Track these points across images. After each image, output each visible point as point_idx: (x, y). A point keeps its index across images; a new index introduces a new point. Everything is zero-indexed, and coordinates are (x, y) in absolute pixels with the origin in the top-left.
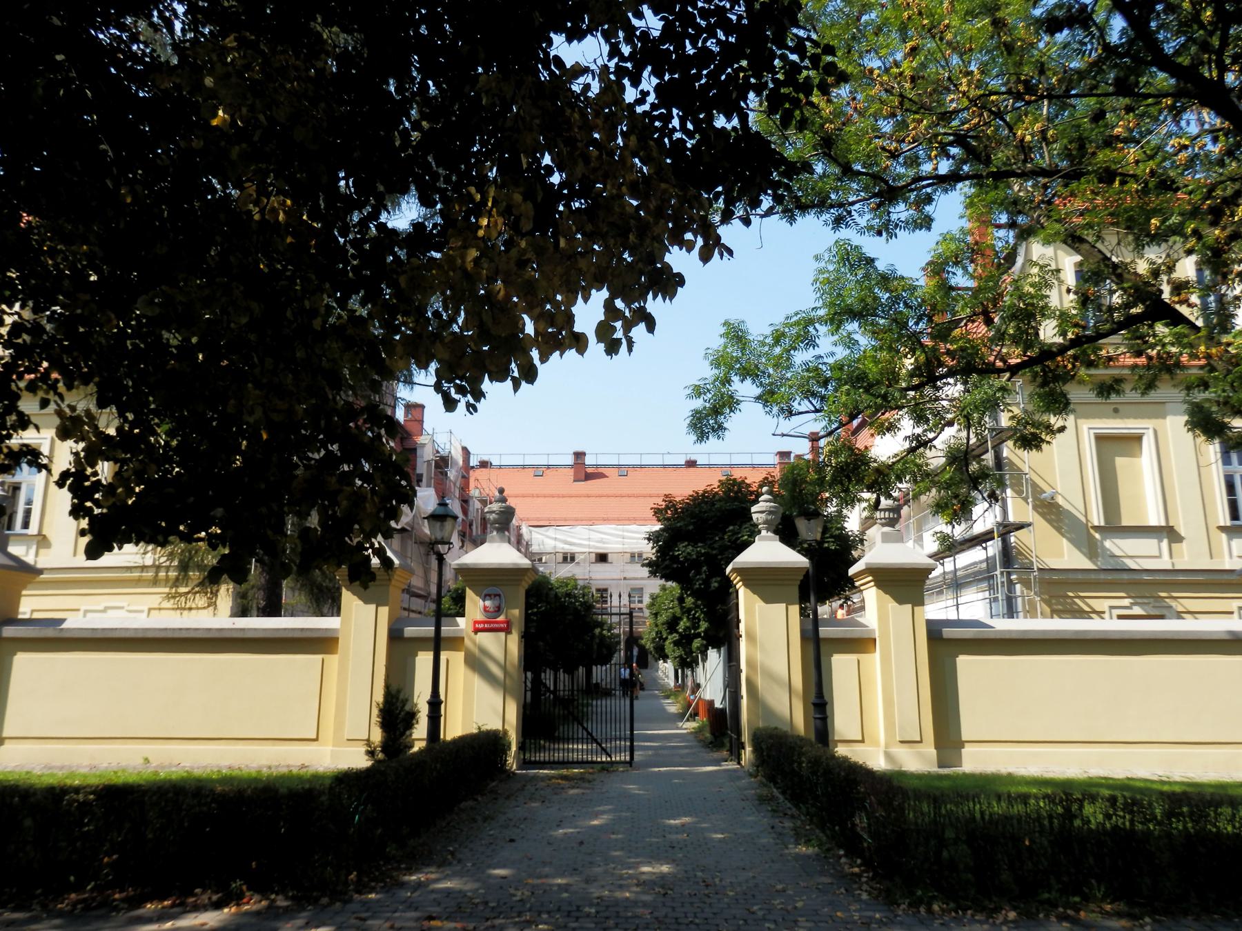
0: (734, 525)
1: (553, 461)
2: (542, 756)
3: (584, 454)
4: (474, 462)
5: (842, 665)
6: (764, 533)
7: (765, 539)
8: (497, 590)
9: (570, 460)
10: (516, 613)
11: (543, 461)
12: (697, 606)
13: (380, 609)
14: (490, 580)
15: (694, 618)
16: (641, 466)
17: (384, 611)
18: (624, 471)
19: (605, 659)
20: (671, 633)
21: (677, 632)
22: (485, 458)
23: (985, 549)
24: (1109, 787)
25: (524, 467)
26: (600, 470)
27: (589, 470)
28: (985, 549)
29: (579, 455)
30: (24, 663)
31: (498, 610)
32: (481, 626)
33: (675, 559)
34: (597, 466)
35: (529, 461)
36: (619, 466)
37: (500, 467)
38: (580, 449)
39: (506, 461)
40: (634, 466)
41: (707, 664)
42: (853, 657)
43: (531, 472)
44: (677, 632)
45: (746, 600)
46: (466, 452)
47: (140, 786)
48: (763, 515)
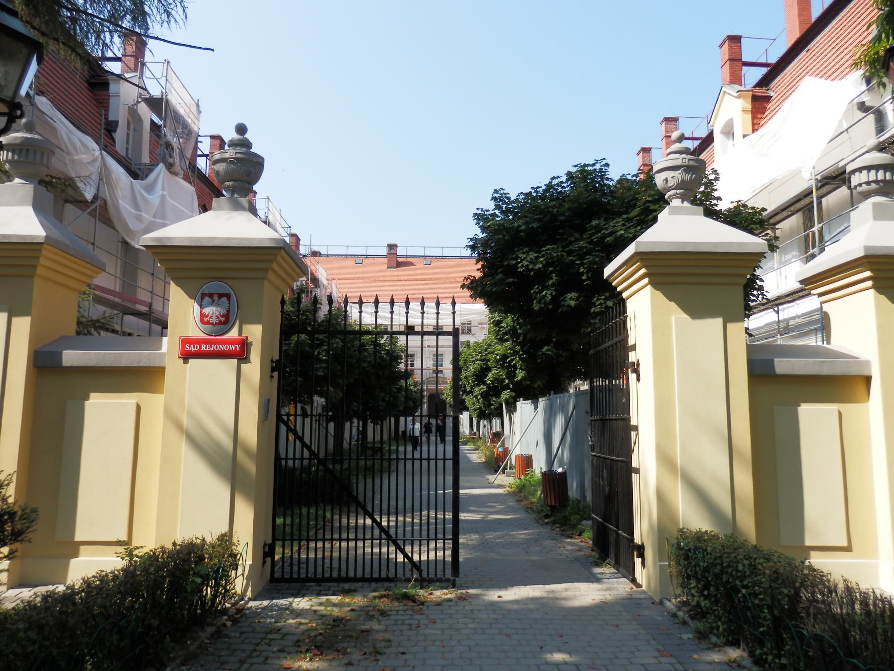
0: (599, 219)
2: (313, 552)
3: (396, 246)
5: (815, 419)
6: (676, 202)
7: (676, 211)
8: (224, 288)
9: (384, 251)
10: (255, 332)
12: (515, 353)
13: (15, 320)
14: (216, 272)
15: (510, 366)
16: (442, 257)
17: (23, 325)
18: (428, 261)
19: (409, 411)
20: (479, 385)
21: (485, 383)
23: (777, 312)
25: (347, 256)
26: (409, 260)
27: (400, 260)
28: (777, 312)
31: (225, 322)
32: (194, 348)
33: (512, 271)
34: (407, 256)
35: (351, 252)
36: (424, 257)
38: (392, 242)
40: (436, 257)
41: (516, 417)
42: (832, 408)
43: (353, 260)
44: (485, 383)
45: (645, 311)
48: (677, 174)
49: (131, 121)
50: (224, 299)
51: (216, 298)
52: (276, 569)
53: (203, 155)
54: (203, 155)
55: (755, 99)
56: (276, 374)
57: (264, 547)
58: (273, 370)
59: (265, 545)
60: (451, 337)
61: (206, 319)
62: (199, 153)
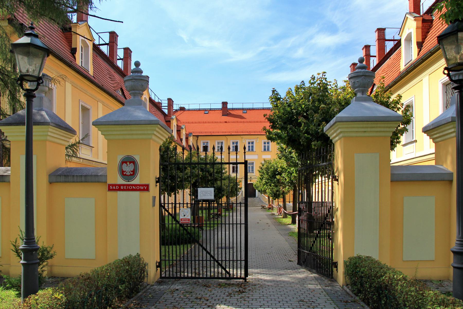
1: (213, 107)
4: (175, 107)
9: (220, 106)
11: (208, 107)
22: (182, 106)
24: (68, 182)
25: (200, 110)
29: (225, 104)
30: (434, 152)
35: (202, 107)
37: (189, 110)
39: (192, 107)
46: (170, 101)
47: (436, 121)
49: (83, 47)
50: (132, 164)
51: (128, 163)
52: (162, 273)
53: (120, 59)
54: (120, 59)
55: (424, 21)
56: (158, 184)
57: (156, 263)
58: (157, 182)
59: (157, 262)
60: (243, 165)
61: (124, 173)
62: (118, 58)
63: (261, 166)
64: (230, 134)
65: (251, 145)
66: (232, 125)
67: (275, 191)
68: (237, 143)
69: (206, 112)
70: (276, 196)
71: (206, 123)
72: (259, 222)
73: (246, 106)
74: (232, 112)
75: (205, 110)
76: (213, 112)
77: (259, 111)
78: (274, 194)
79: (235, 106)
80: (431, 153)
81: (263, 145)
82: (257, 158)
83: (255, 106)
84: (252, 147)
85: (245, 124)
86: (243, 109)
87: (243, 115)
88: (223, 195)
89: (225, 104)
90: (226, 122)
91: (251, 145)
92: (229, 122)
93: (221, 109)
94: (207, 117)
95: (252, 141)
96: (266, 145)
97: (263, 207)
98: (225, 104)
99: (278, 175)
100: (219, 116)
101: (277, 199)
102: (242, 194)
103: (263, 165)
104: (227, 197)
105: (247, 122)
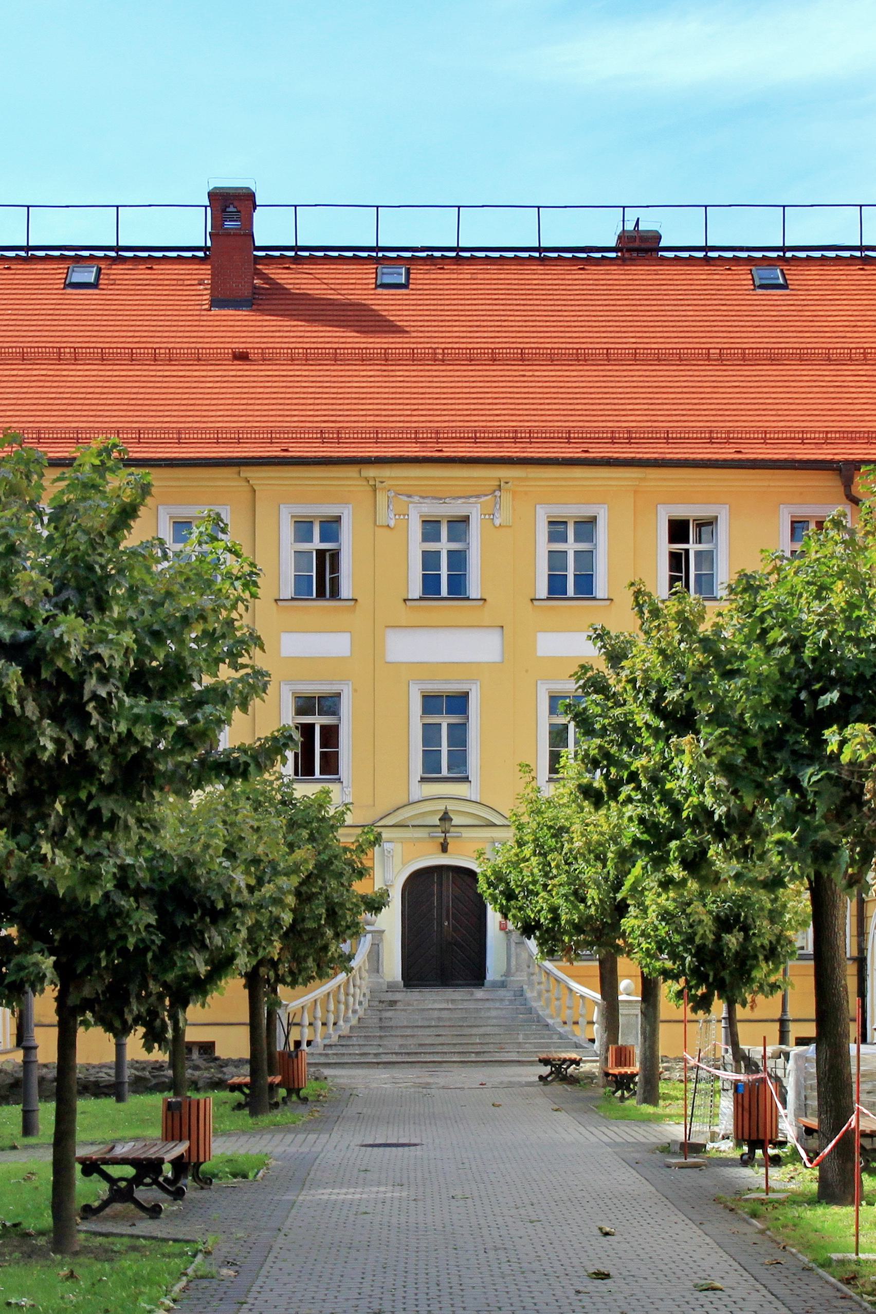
1: (140, 231)
9: (192, 229)
11: (94, 231)
35: (51, 231)
63: (601, 665)
64: (274, 451)
65: (444, 546)
66: (293, 383)
67: (706, 931)
68: (331, 528)
69: (77, 278)
70: (719, 968)
71: (76, 358)
72: (601, 1256)
73: (400, 232)
74: (289, 279)
75: (70, 256)
76: (141, 272)
77: (510, 275)
78: (700, 952)
79: (318, 231)
80: (193, 1027)
81: (543, 546)
82: (495, 657)
83: (480, 233)
84: (458, 560)
85: (400, 371)
86: (376, 256)
87: (386, 304)
88: (221, 964)
89: (231, 207)
90: (241, 357)
91: (444, 546)
92: (265, 359)
93: (205, 256)
94: (84, 318)
95: (456, 509)
96: (571, 546)
97: (560, 1073)
98: (231, 207)
99: (840, 715)
100: (186, 312)
101: (719, 1007)
102: (375, 956)
103: (615, 658)
104: (253, 980)
105: (414, 358)
